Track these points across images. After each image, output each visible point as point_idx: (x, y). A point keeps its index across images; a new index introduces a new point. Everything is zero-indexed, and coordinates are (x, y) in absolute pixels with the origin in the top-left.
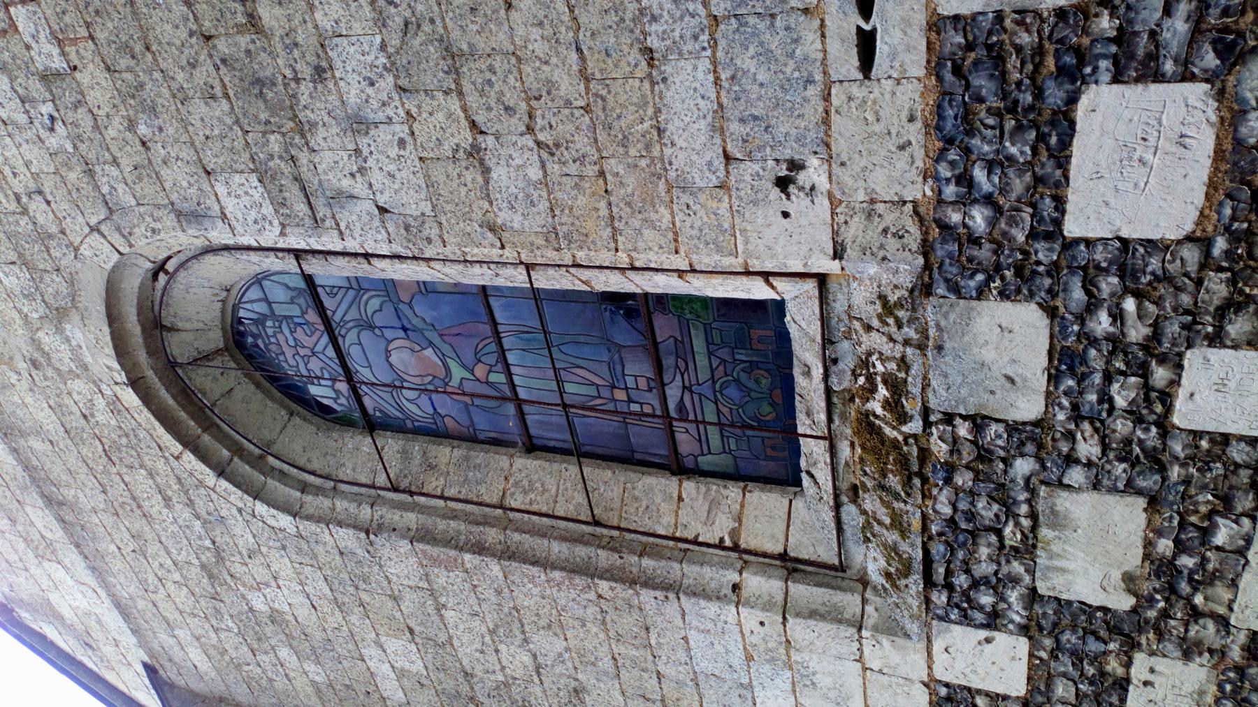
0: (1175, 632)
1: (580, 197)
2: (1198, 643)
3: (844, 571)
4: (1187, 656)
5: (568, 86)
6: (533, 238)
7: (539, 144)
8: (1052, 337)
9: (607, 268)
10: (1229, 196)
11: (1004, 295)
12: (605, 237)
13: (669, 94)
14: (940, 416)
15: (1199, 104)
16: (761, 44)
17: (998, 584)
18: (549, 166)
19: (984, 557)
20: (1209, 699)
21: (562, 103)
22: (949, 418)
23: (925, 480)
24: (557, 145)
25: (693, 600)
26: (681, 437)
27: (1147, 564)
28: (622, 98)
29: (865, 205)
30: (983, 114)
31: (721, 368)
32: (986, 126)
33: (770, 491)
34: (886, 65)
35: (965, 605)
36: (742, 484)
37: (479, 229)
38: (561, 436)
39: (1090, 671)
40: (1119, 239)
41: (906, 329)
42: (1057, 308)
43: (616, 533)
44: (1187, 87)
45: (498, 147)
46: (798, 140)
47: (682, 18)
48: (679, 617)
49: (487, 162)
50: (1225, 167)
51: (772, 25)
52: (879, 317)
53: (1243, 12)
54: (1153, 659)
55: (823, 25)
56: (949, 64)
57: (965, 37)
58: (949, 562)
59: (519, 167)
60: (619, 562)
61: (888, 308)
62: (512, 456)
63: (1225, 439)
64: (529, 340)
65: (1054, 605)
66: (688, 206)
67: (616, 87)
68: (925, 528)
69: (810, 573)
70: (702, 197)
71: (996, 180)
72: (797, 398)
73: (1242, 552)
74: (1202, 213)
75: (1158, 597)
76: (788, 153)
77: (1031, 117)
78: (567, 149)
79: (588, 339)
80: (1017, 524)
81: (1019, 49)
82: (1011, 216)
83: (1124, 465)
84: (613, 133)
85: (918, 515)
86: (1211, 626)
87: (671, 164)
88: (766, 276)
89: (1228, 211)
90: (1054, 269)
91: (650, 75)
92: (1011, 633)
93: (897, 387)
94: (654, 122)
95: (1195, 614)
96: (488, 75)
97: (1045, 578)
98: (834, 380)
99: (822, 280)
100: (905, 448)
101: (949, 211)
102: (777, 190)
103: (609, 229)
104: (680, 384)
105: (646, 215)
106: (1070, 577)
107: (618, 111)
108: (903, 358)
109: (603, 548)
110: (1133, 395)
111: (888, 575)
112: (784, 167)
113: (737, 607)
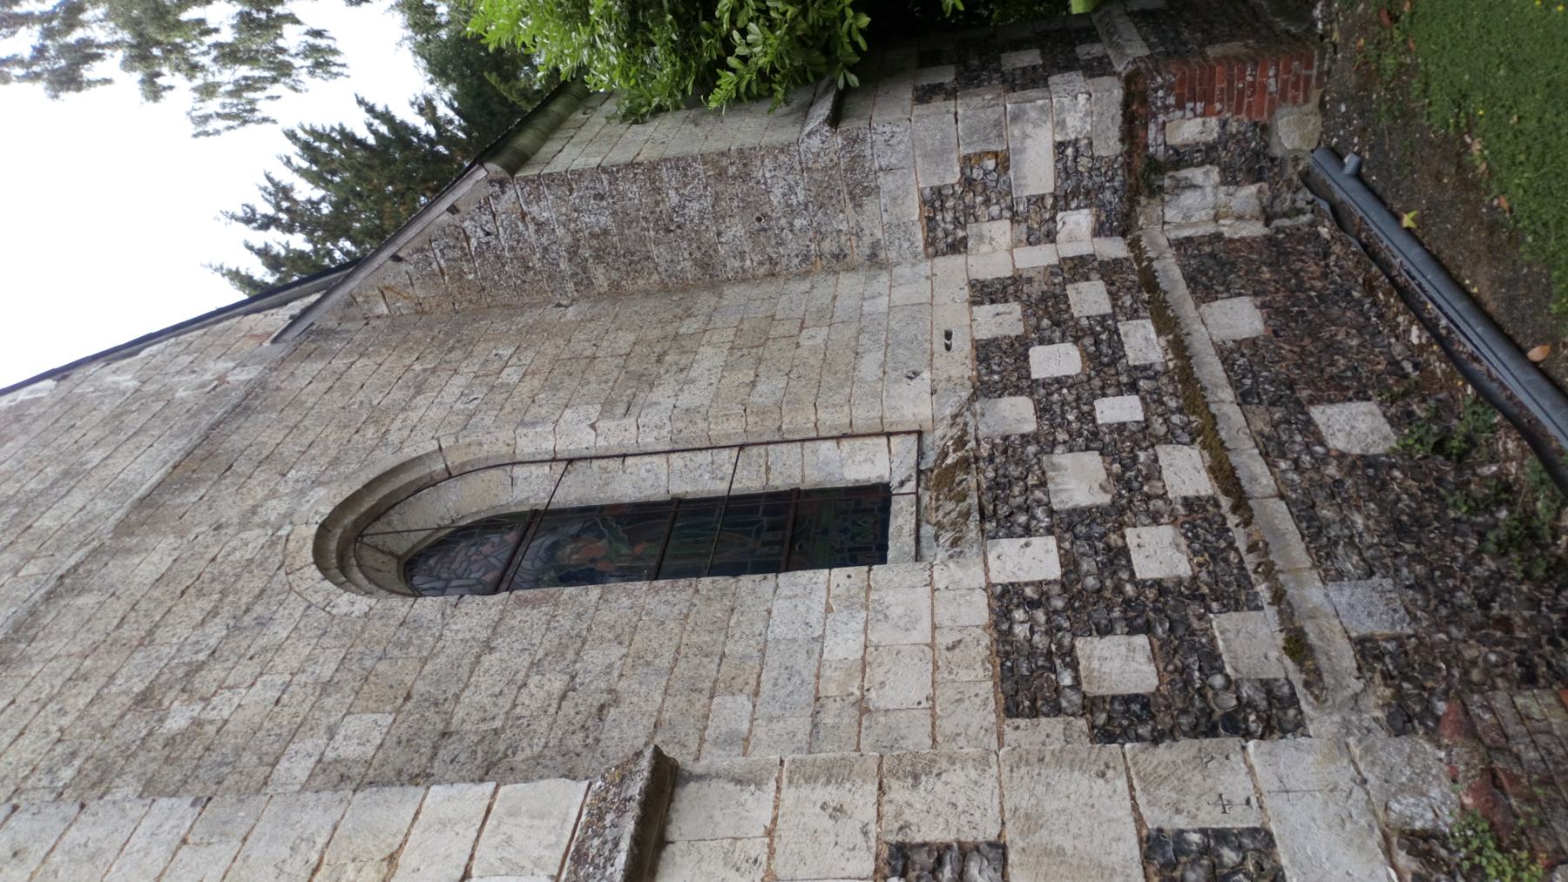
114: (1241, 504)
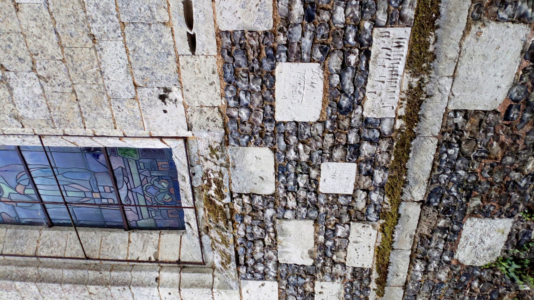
0: (328, 271)
1: (63, 102)
2: (336, 274)
3: (205, 264)
4: (333, 280)
5: (52, 49)
6: (40, 122)
7: (39, 77)
8: (275, 160)
9: (82, 136)
10: (330, 105)
11: (256, 144)
12: (78, 121)
13: (104, 56)
14: (237, 195)
15: (317, 71)
16: (146, 36)
17: (264, 261)
18: (45, 87)
19: (258, 251)
20: (342, 296)
21: (50, 57)
22: (240, 195)
23: (233, 222)
24: (49, 78)
25: (137, 288)
26: (128, 213)
27: (316, 246)
28: (81, 57)
29: (199, 108)
30: (241, 72)
31: (145, 180)
32: (243, 77)
33: (172, 233)
34: (201, 49)
35: (253, 272)
36: (159, 231)
37: (9, 118)
38: (65, 218)
39: (301, 291)
40: (295, 122)
41: (220, 160)
42: (276, 149)
43: (98, 262)
44: (312, 64)
45: (16, 77)
46: (167, 79)
47: (107, 22)
48: (131, 297)
49: (11, 85)
50: (327, 95)
51: (150, 28)
52: (210, 155)
53: (329, 37)
54: (322, 283)
55: (172, 30)
56: (226, 51)
57: (231, 40)
58: (245, 255)
59: (29, 88)
60: (100, 275)
61: (213, 151)
62: (41, 230)
63: (337, 196)
64: (45, 171)
65: (285, 267)
66: (119, 107)
67: (77, 51)
68: (235, 242)
69: (191, 267)
70: (125, 103)
71: (249, 99)
72: (181, 191)
73: (347, 238)
74: (321, 112)
75: (321, 258)
76: (163, 85)
77: (259, 74)
78: (54, 79)
79: (78, 170)
80: (269, 236)
81: (252, 47)
82: (256, 113)
83: (305, 209)
84: (77, 72)
85: (232, 237)
86: (339, 266)
87: (108, 88)
88: (161, 138)
89: (330, 111)
90: (274, 133)
91: (94, 47)
92: (271, 281)
93: (219, 184)
94: (98, 68)
95: (334, 263)
96: (8, 43)
97: (281, 256)
98: (194, 182)
99: (185, 139)
100: (224, 209)
101: (232, 110)
102: (160, 101)
103: (80, 118)
104: (126, 188)
105: (98, 111)
106: (290, 255)
107: (80, 62)
108: (220, 172)
109: (91, 270)
110: (305, 181)
111: (222, 264)
112: (162, 90)
113: (158, 288)
114: (382, 282)
